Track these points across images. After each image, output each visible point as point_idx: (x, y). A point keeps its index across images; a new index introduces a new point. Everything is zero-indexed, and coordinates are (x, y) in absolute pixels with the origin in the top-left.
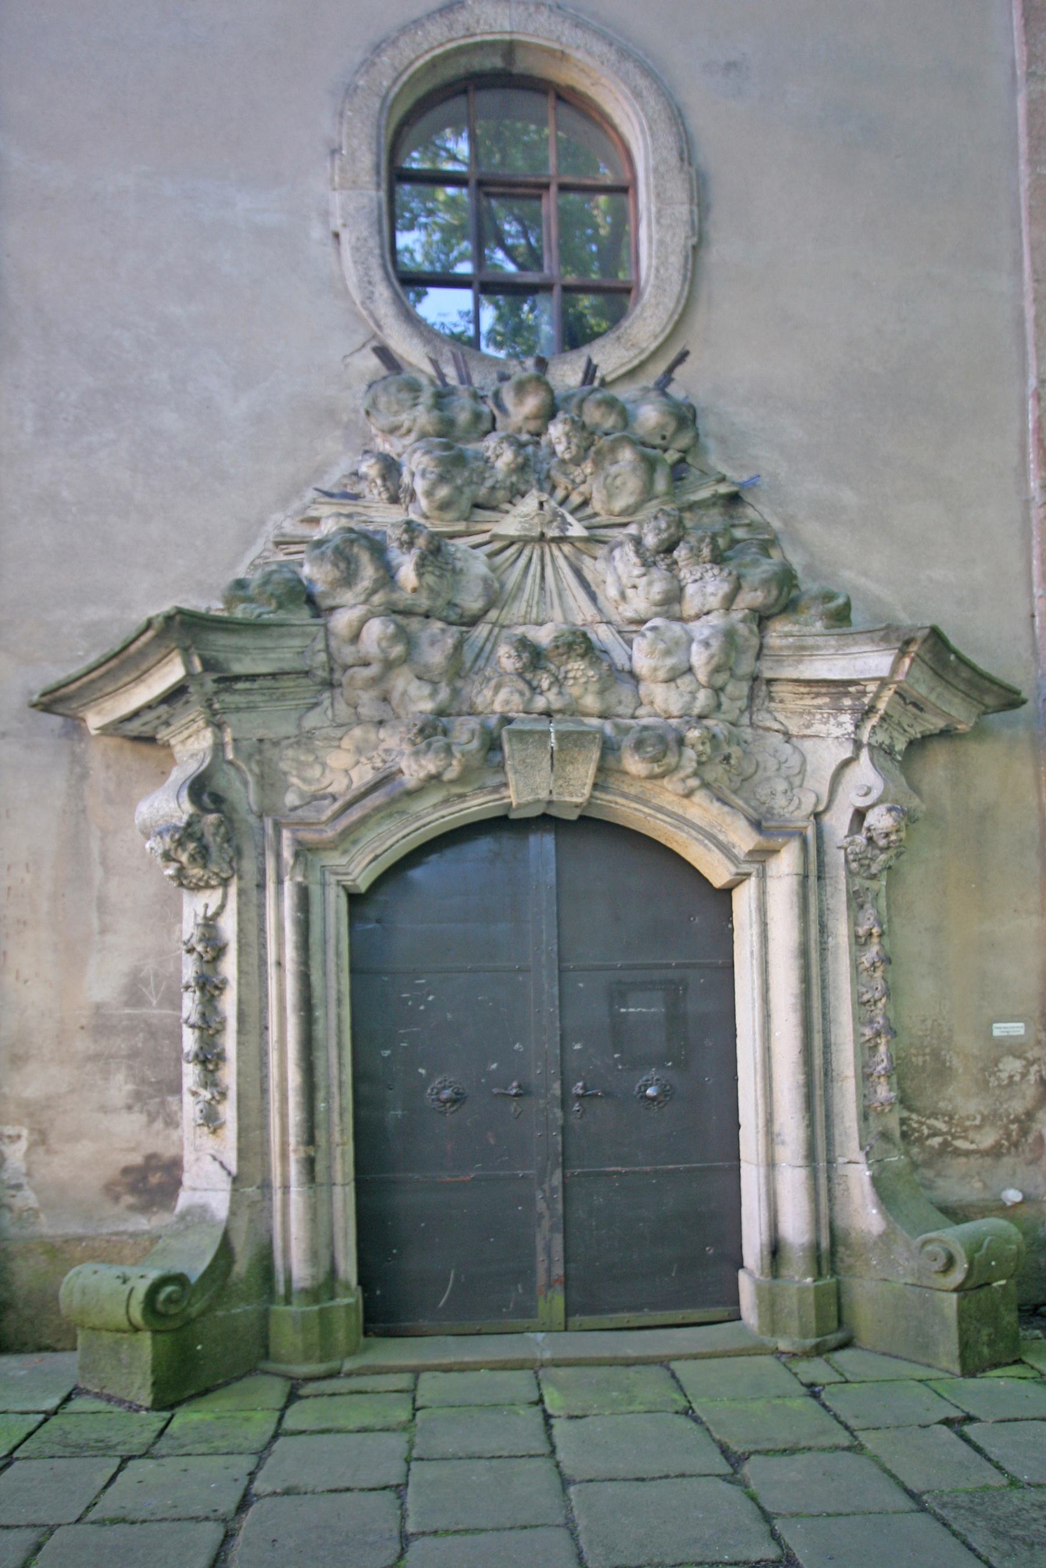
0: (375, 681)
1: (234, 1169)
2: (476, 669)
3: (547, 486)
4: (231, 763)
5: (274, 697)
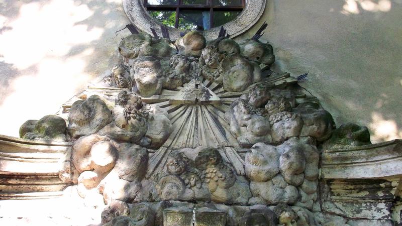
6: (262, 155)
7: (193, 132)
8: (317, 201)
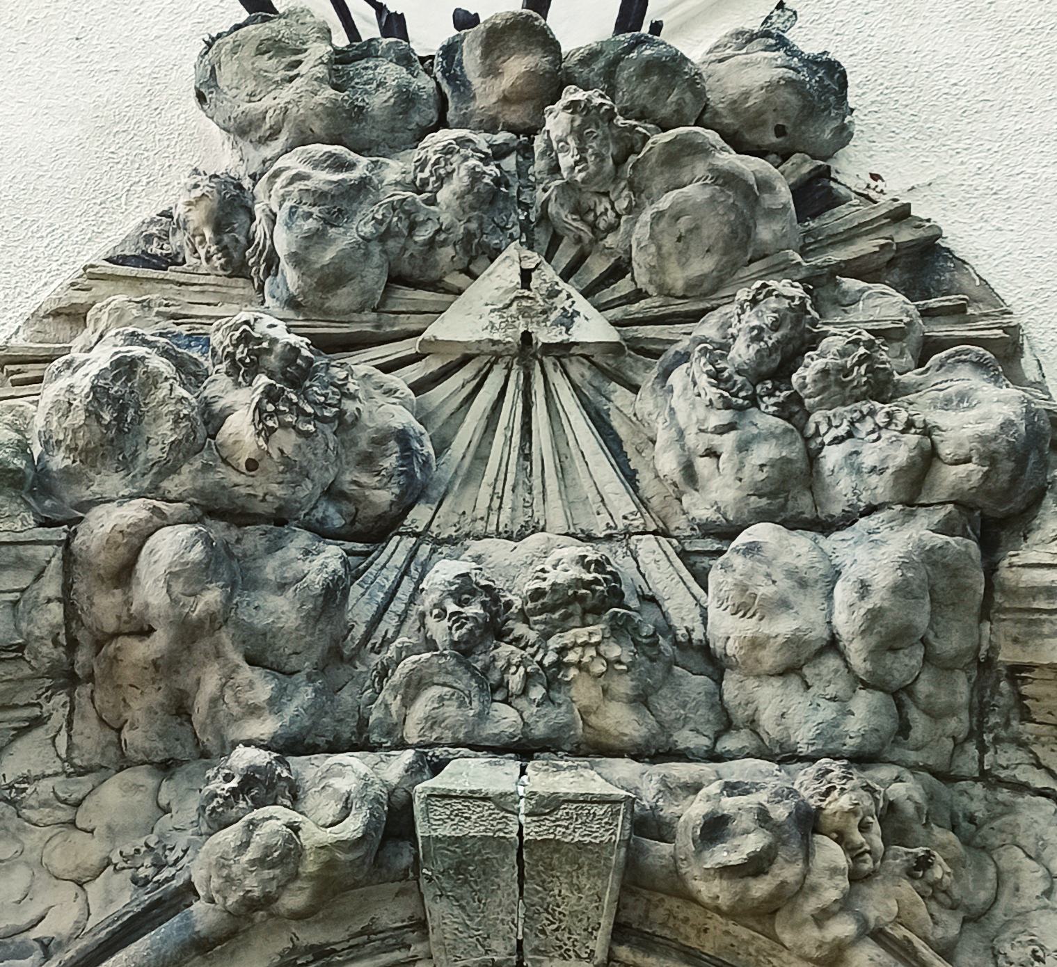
0: (163, 667)
3: (542, 237)
6: (768, 575)
7: (512, 468)
8: (966, 740)
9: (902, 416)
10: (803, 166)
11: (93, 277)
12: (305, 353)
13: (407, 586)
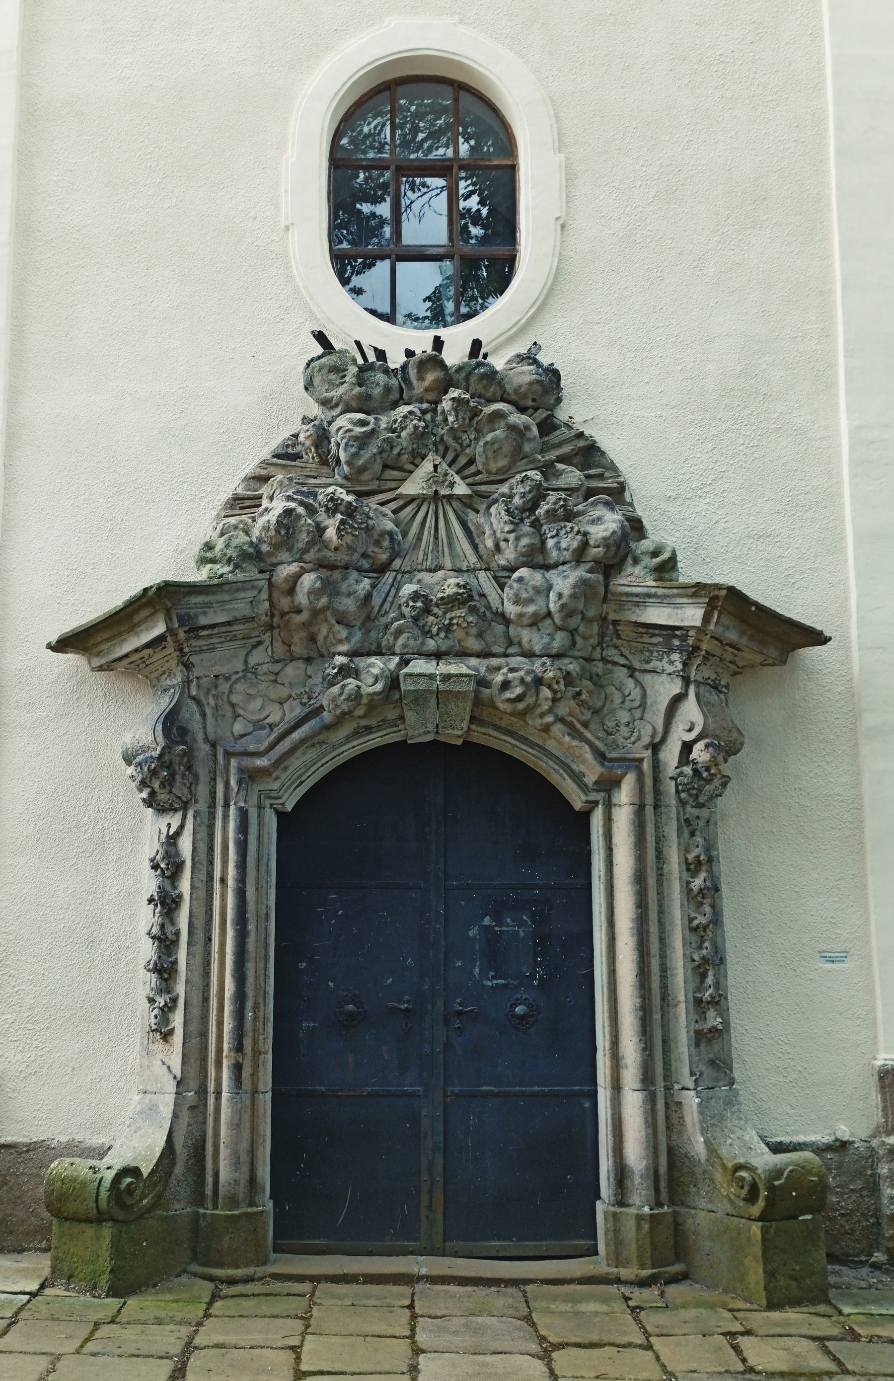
0: (305, 625)
1: (179, 1075)
2: (383, 612)
3: (441, 448)
4: (193, 698)
5: (228, 638)
7: (431, 543)
9: (576, 529)
10: (542, 414)
11: (268, 464)
12: (354, 504)
13: (393, 591)
